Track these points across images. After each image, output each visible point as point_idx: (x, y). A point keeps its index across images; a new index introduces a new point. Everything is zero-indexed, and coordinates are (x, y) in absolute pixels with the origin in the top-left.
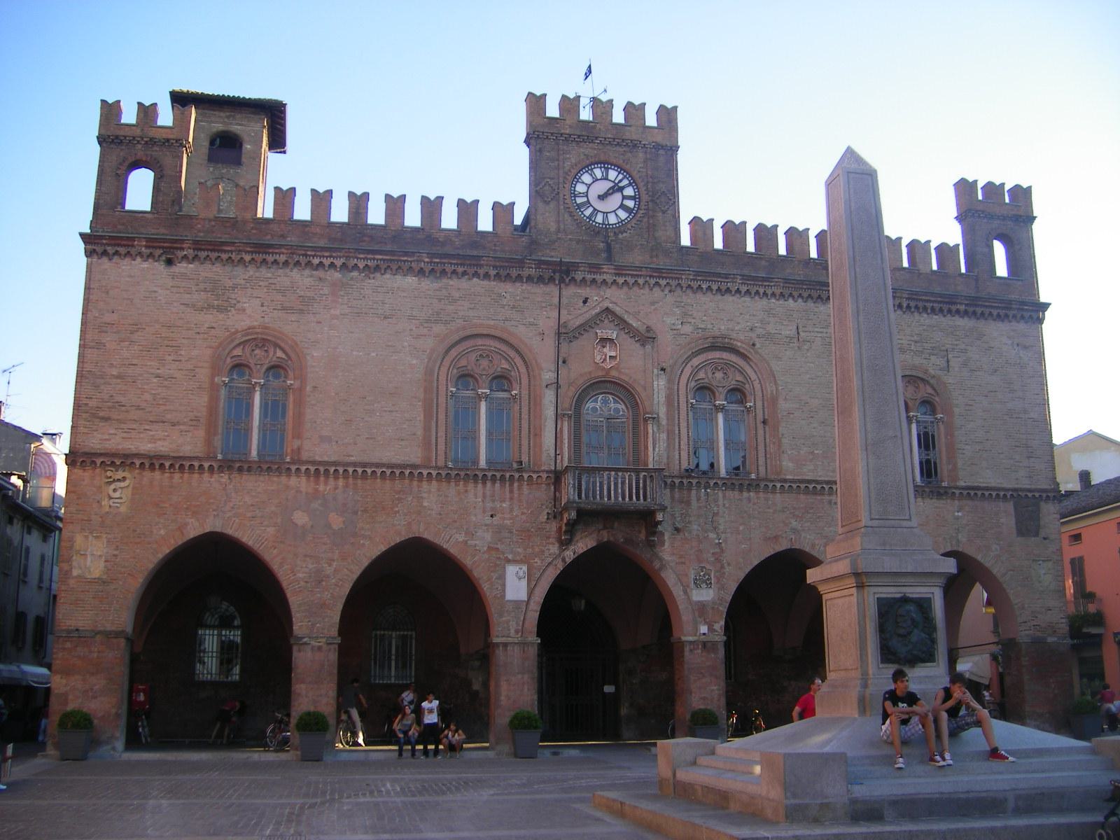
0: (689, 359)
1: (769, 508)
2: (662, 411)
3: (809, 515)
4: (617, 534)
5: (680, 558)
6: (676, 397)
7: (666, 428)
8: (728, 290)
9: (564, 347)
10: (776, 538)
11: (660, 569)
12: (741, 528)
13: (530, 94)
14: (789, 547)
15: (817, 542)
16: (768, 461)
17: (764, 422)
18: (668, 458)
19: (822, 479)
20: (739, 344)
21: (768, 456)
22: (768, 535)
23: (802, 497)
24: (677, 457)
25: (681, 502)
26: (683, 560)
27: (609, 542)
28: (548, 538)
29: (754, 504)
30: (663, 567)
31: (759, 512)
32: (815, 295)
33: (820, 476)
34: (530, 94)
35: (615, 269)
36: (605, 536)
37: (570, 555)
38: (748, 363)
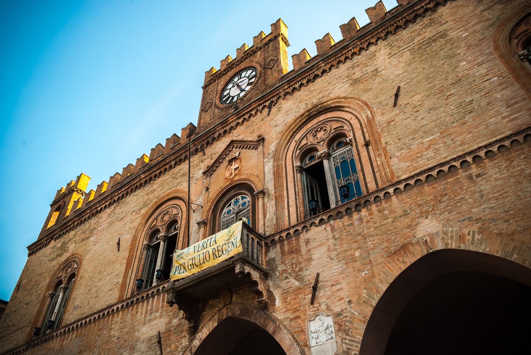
0: (293, 136)
1: (387, 218)
2: (270, 186)
3: (444, 204)
4: (233, 308)
5: (295, 312)
6: (285, 180)
7: (274, 196)
8: (316, 77)
9: (203, 114)
10: (404, 248)
11: (274, 332)
12: (357, 254)
13: (191, 123)
14: (425, 253)
15: (466, 231)
16: (377, 174)
17: (367, 145)
18: (277, 219)
19: (450, 158)
20: (329, 103)
21: (376, 170)
22: (393, 249)
23: (427, 189)
24: (287, 214)
25: (291, 252)
26: (297, 314)
27: (228, 318)
28: (182, 332)
29: (368, 222)
30: (277, 328)
31: (376, 228)
32: (391, 29)
33: (445, 158)
34: (191, 123)
35: (236, 116)
36: (225, 313)
37: (197, 343)
38: (343, 111)
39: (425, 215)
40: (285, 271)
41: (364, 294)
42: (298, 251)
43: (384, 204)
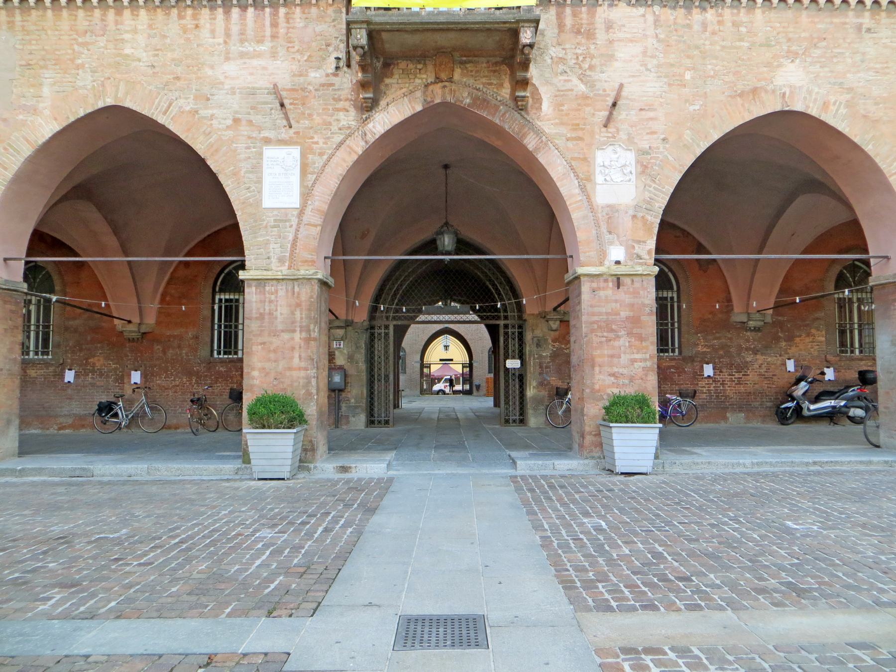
39: (792, 56)
40: (562, 60)
41: (688, 135)
42: (590, 35)
43: (743, 16)
